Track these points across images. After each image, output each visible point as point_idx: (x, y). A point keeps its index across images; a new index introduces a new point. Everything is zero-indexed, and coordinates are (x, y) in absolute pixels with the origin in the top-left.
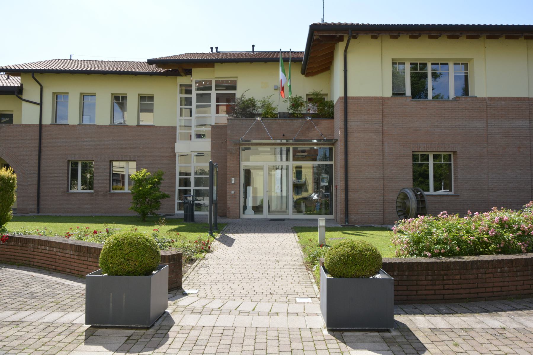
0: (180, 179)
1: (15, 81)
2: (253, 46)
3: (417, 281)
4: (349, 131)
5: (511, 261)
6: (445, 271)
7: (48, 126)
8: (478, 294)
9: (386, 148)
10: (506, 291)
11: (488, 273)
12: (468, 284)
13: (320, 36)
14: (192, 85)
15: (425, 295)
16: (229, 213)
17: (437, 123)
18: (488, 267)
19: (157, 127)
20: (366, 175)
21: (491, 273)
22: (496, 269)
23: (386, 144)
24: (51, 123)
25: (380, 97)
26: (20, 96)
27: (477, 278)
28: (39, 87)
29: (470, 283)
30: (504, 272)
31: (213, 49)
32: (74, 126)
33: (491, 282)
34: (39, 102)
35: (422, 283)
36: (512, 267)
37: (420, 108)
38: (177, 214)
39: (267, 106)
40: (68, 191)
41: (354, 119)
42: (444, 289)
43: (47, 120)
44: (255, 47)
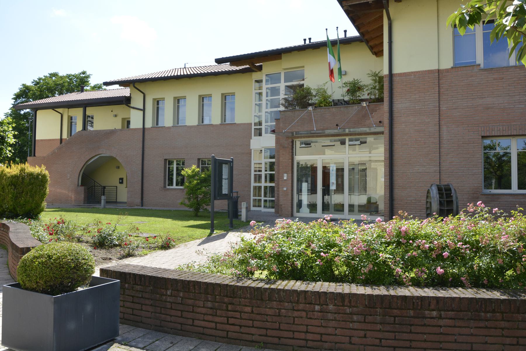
0: (255, 175)
1: (126, 92)
2: (345, 31)
3: (193, 306)
4: (396, 114)
5: (342, 296)
6: (230, 298)
7: (149, 129)
8: (279, 339)
9: (445, 134)
10: (330, 342)
11: (298, 310)
12: (264, 321)
13: (350, 6)
14: (262, 80)
15: (204, 328)
16: (281, 211)
17: (518, 96)
18: (298, 300)
19: (238, 124)
20: (417, 169)
21: (304, 311)
22: (312, 306)
23: (444, 129)
24: (151, 126)
25: (436, 70)
26: (129, 105)
27: (279, 315)
28: (142, 95)
29: (267, 321)
30: (327, 312)
31: (306, 41)
32: (169, 128)
33: (302, 325)
34: (142, 108)
35: (199, 310)
36: (342, 306)
37: (492, 79)
38: (252, 210)
39: (322, 93)
40: (165, 187)
41: (401, 100)
42: (228, 324)
43: (149, 124)
44: (347, 33)
